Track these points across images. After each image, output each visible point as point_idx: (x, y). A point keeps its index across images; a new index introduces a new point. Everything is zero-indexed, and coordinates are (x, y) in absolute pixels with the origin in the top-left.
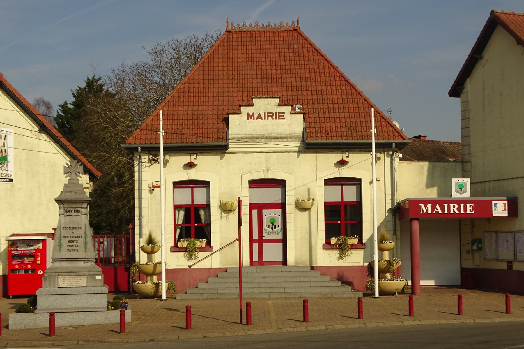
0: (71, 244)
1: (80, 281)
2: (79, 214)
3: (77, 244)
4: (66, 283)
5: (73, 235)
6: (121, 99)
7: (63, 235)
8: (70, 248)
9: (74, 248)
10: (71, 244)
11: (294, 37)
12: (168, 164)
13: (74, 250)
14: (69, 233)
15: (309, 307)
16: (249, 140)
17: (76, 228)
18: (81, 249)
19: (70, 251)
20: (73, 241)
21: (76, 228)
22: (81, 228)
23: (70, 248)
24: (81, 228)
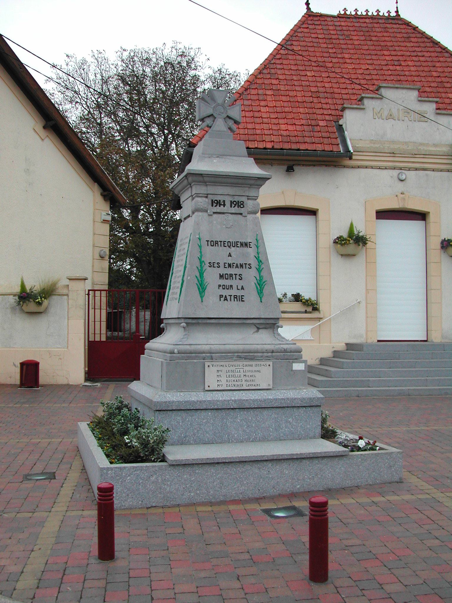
0: (227, 283)
1: (257, 374)
2: (242, 210)
3: (240, 283)
4: (224, 379)
5: (230, 260)
6: (122, 79)
7: (207, 259)
8: (225, 293)
9: (234, 292)
10: (227, 283)
11: (396, 21)
12: (34, 283)
13: (235, 297)
14: (220, 254)
15: (330, 519)
16: (389, 155)
17: (235, 244)
18: (251, 295)
19: (226, 299)
20: (231, 275)
21: (235, 244)
22: (246, 245)
23: (225, 293)
24: (246, 245)
